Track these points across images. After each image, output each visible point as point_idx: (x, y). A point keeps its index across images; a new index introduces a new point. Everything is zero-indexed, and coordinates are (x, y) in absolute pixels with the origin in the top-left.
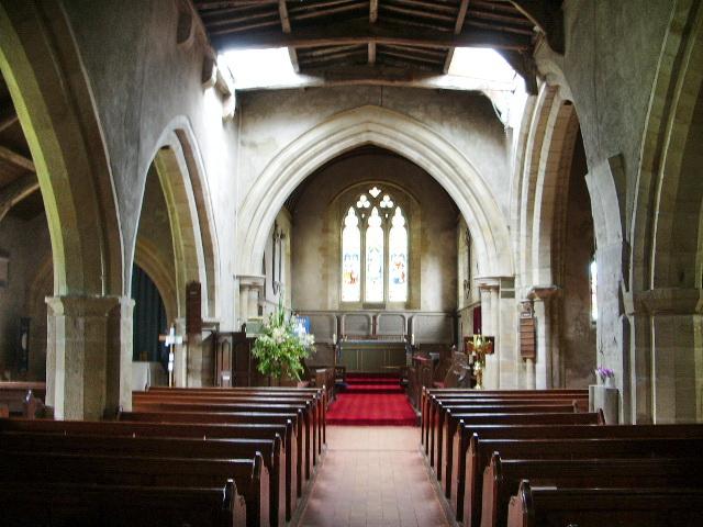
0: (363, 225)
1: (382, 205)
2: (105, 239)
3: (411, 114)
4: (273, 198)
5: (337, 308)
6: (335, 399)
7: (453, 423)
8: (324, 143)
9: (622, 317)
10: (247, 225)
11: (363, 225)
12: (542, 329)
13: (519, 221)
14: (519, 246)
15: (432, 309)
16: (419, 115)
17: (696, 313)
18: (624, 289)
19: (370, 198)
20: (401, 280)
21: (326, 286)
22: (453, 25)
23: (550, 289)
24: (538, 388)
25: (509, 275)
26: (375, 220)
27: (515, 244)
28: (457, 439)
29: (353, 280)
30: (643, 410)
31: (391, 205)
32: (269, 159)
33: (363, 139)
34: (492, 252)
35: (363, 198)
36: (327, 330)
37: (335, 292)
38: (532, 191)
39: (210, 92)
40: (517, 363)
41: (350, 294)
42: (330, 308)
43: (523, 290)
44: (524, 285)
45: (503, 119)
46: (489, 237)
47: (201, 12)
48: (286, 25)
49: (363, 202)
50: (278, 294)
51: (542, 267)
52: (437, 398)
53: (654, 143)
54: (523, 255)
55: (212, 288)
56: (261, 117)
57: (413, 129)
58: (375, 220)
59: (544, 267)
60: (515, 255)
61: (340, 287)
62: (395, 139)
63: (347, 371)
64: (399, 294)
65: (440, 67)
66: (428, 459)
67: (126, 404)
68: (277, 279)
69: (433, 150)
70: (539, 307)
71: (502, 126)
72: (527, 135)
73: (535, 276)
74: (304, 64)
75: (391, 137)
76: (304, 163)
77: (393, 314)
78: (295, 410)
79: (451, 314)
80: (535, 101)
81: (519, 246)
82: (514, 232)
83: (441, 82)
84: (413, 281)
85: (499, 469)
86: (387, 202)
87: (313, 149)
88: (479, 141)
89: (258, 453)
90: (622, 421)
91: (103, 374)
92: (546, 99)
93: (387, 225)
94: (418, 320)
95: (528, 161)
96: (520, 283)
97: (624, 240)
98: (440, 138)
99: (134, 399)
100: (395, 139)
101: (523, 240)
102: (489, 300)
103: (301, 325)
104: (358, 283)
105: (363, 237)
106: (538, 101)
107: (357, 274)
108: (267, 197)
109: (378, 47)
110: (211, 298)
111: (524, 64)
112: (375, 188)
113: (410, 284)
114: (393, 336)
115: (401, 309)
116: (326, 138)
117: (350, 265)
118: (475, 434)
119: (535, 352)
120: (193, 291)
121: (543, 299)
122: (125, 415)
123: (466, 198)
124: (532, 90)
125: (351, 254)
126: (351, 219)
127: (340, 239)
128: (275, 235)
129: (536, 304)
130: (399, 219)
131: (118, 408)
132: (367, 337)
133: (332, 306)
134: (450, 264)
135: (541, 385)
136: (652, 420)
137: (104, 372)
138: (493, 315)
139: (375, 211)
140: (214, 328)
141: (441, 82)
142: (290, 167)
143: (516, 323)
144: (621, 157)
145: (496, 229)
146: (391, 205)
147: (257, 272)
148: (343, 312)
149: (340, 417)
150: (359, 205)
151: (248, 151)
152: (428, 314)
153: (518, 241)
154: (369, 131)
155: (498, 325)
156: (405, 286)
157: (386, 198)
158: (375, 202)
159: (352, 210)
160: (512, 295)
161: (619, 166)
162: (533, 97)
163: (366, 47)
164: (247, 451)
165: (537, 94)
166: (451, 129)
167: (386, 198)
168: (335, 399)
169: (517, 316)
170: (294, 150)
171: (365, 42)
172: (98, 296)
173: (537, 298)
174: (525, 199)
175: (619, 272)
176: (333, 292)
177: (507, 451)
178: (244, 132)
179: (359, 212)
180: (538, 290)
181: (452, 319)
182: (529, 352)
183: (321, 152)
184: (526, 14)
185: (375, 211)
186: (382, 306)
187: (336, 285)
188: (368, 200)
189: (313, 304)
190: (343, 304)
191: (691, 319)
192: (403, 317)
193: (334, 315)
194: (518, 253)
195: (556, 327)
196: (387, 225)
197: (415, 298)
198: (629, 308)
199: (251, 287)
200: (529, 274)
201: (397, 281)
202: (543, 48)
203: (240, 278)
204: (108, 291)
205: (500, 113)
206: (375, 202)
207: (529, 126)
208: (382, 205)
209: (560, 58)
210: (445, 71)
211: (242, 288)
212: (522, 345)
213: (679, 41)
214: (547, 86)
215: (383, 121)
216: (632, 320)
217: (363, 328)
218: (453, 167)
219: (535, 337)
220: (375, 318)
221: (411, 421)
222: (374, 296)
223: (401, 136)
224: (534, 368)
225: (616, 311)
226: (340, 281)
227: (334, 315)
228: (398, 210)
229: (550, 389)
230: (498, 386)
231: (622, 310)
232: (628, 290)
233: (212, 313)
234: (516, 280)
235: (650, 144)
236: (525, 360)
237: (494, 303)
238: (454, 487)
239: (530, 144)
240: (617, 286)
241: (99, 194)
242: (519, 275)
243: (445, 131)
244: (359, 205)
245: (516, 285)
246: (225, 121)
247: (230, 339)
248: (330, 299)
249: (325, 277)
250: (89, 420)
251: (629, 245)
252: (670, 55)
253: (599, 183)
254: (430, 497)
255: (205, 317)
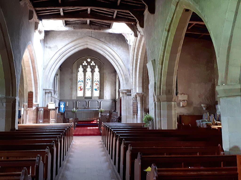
0: (85, 71)
1: (92, 64)
2: (12, 83)
3: (101, 40)
4: (56, 65)
5: (76, 99)
6: (75, 129)
7: (109, 129)
8: (73, 48)
9: (154, 102)
10: (48, 73)
11: (85, 71)
12: (139, 106)
13: (133, 73)
14: (132, 80)
15: (108, 99)
16: (103, 40)
17: (173, 101)
18: (155, 95)
19: (87, 62)
20: (97, 89)
21: (72, 91)
22: (113, 15)
23: (141, 94)
24: (138, 123)
25: (129, 89)
26: (89, 69)
27: (131, 80)
28: (114, 138)
29: (81, 90)
30: (159, 127)
31: (94, 64)
32: (55, 52)
33: (85, 47)
34: (124, 82)
35: (85, 62)
36: (72, 107)
37: (75, 93)
38: (136, 64)
39: (37, 31)
40: (132, 116)
41: (80, 94)
42: (73, 99)
43: (133, 94)
44: (134, 92)
45: (128, 43)
46: (124, 78)
47: (36, 11)
48: (62, 14)
49: (85, 63)
50: (55, 94)
51: (139, 87)
52: (112, 129)
53: (162, 58)
54: (134, 83)
55: (36, 93)
56: (52, 38)
57: (101, 44)
58: (89, 69)
59: (140, 87)
60: (131, 83)
61: (77, 92)
62: (96, 47)
63: (79, 120)
64: (96, 94)
65: (109, 26)
66: (103, 143)
67: (17, 128)
68: (55, 89)
69: (108, 52)
70: (138, 98)
71: (128, 45)
72: (135, 48)
73: (137, 90)
74: (67, 24)
75: (94, 47)
76: (67, 54)
77: (95, 101)
78: (60, 134)
79: (114, 101)
80: (137, 39)
81: (132, 80)
82: (131, 76)
83: (110, 31)
84: (102, 90)
85: (124, 144)
86: (93, 63)
87: (70, 49)
88: (121, 49)
89: (53, 141)
90: (154, 129)
91: (10, 119)
92: (140, 38)
93: (93, 71)
94: (103, 103)
95: (135, 55)
96: (133, 92)
97: (155, 82)
98: (109, 47)
99: (18, 127)
100: (96, 47)
101: (134, 79)
102: (124, 97)
103: (62, 104)
104: (83, 90)
105: (85, 75)
106: (138, 39)
107: (82, 87)
108: (54, 65)
109: (90, 21)
110: (36, 97)
111: (133, 28)
112: (89, 59)
113: (100, 91)
114: (94, 108)
115: (97, 99)
116: (74, 46)
117: (80, 84)
118: (124, 139)
119: (137, 112)
120: (30, 95)
121: (140, 96)
122: (17, 130)
123: (117, 66)
124: (136, 36)
125: (81, 81)
126: (81, 69)
127: (77, 75)
128: (57, 75)
129: (137, 98)
130: (97, 70)
131: (15, 129)
132: (85, 108)
133: (74, 98)
134: (114, 83)
135: (139, 122)
136: (162, 129)
137: (11, 118)
138: (125, 101)
139: (89, 66)
140: (37, 106)
141: (110, 31)
142: (62, 55)
143: (131, 103)
144: (154, 60)
145: (126, 75)
146: (94, 64)
147: (51, 88)
148: (77, 100)
149: (77, 133)
150: (84, 64)
151: (48, 50)
152: (106, 101)
153: (132, 79)
154: (87, 44)
155: (126, 104)
156: (98, 92)
157: (93, 62)
158: (89, 63)
159: (81, 66)
160: (130, 95)
161: (154, 62)
162: (136, 38)
163: (87, 10)
164: (56, 137)
165: (137, 37)
166: (113, 44)
167: (93, 62)
168: (75, 129)
169: (132, 102)
170: (64, 49)
171: (87, 8)
172: (10, 97)
173: (138, 96)
174: (134, 67)
175: (154, 90)
176: (74, 93)
177: (126, 140)
178: (47, 43)
179: (83, 67)
180: (137, 94)
181: (114, 103)
182: (135, 112)
183: (72, 50)
184: (134, 16)
185: (89, 66)
186: (90, 98)
187: (75, 91)
188: (87, 63)
189: (67, 98)
190: (77, 97)
191: (171, 103)
192: (86, 101)
193: (75, 101)
194: (132, 83)
195: (144, 105)
196: (93, 71)
197: (102, 95)
198: (156, 100)
199: (48, 93)
200: (135, 89)
201: (96, 90)
202: (138, 25)
203: (45, 90)
204: (12, 96)
205: (127, 41)
206: (89, 63)
207: (135, 45)
208: (92, 64)
209: (143, 29)
210: (111, 27)
211: (46, 93)
212: (133, 110)
213: (167, 33)
214: (140, 34)
215: (92, 42)
216: (156, 103)
217: (83, 106)
218: (113, 56)
219: (137, 108)
220: (88, 102)
221: (99, 134)
222: (88, 94)
223: (97, 46)
224: (137, 117)
225: (153, 100)
226: (77, 90)
227: (75, 101)
228: (97, 66)
229: (142, 123)
230: (126, 122)
231: (154, 101)
232: (156, 95)
233: (36, 101)
234: (132, 91)
235: (161, 57)
236: (134, 115)
237: (125, 97)
238: (108, 149)
239: (136, 51)
240: (153, 94)
241: (11, 68)
242: (133, 89)
243: (111, 46)
244: (84, 64)
245: (132, 92)
246: (41, 41)
247: (43, 109)
248: (73, 96)
249: (72, 88)
250: (6, 131)
251: (156, 83)
252: (165, 36)
253: (149, 66)
254: (103, 151)
255: (34, 103)
